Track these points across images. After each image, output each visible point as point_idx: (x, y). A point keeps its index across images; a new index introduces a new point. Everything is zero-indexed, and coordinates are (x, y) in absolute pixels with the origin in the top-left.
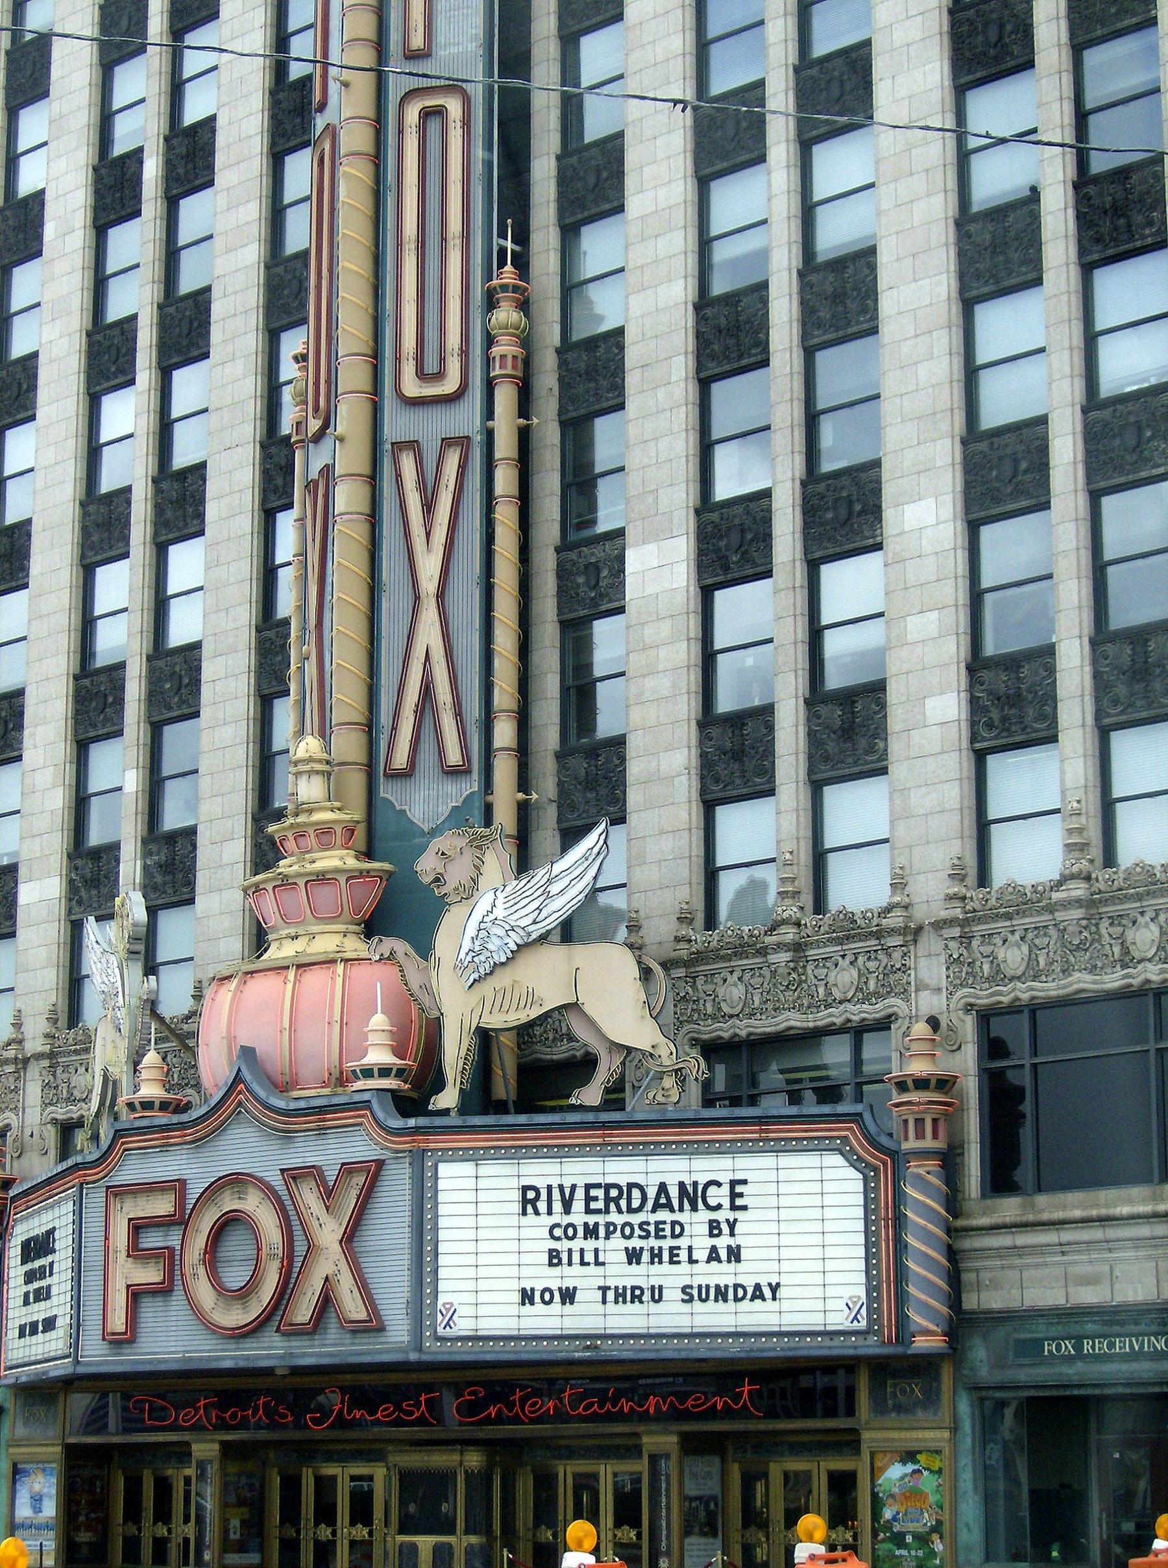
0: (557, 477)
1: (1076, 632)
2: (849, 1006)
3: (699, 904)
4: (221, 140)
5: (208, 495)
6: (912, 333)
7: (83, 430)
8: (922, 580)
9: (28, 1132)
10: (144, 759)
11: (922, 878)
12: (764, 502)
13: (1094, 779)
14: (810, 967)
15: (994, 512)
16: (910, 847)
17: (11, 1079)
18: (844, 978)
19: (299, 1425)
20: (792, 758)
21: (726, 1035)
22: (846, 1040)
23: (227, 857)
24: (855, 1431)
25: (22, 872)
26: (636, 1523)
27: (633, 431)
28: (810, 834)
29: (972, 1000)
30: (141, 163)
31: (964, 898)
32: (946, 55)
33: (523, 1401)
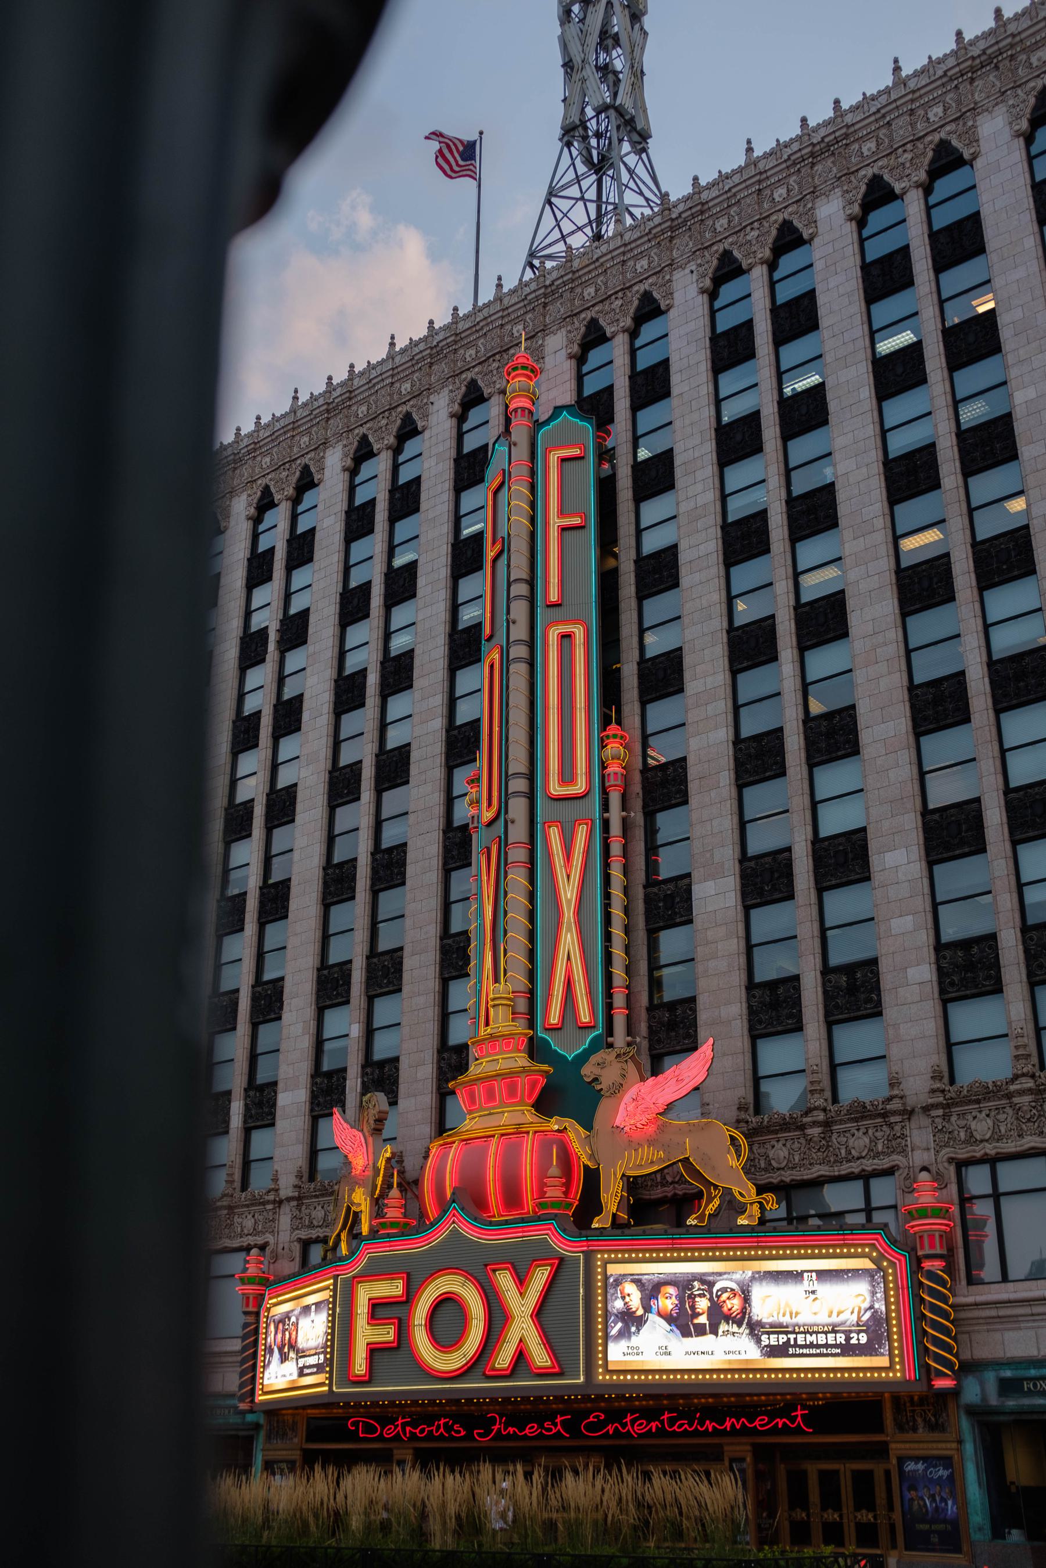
0: (642, 844)
1: (1011, 924)
2: (864, 1161)
3: (751, 1099)
4: (417, 662)
5: (408, 861)
6: (884, 752)
7: (325, 827)
8: (900, 897)
9: (280, 1246)
10: (363, 1017)
11: (911, 1079)
12: (348, 966)
13: (825, 1053)
14: (835, 1135)
15: (945, 855)
16: (902, 1060)
17: (271, 1213)
18: (249, 1223)
19: (469, 1437)
20: (814, 1008)
21: (775, 1181)
22: (986, 1169)
23: (420, 1075)
24: (886, 1444)
25: (281, 1086)
26: (871, 1507)
27: (695, 816)
28: (827, 1054)
29: (953, 1156)
30: (365, 677)
31: (943, 1091)
32: (896, 596)
33: (633, 1421)
